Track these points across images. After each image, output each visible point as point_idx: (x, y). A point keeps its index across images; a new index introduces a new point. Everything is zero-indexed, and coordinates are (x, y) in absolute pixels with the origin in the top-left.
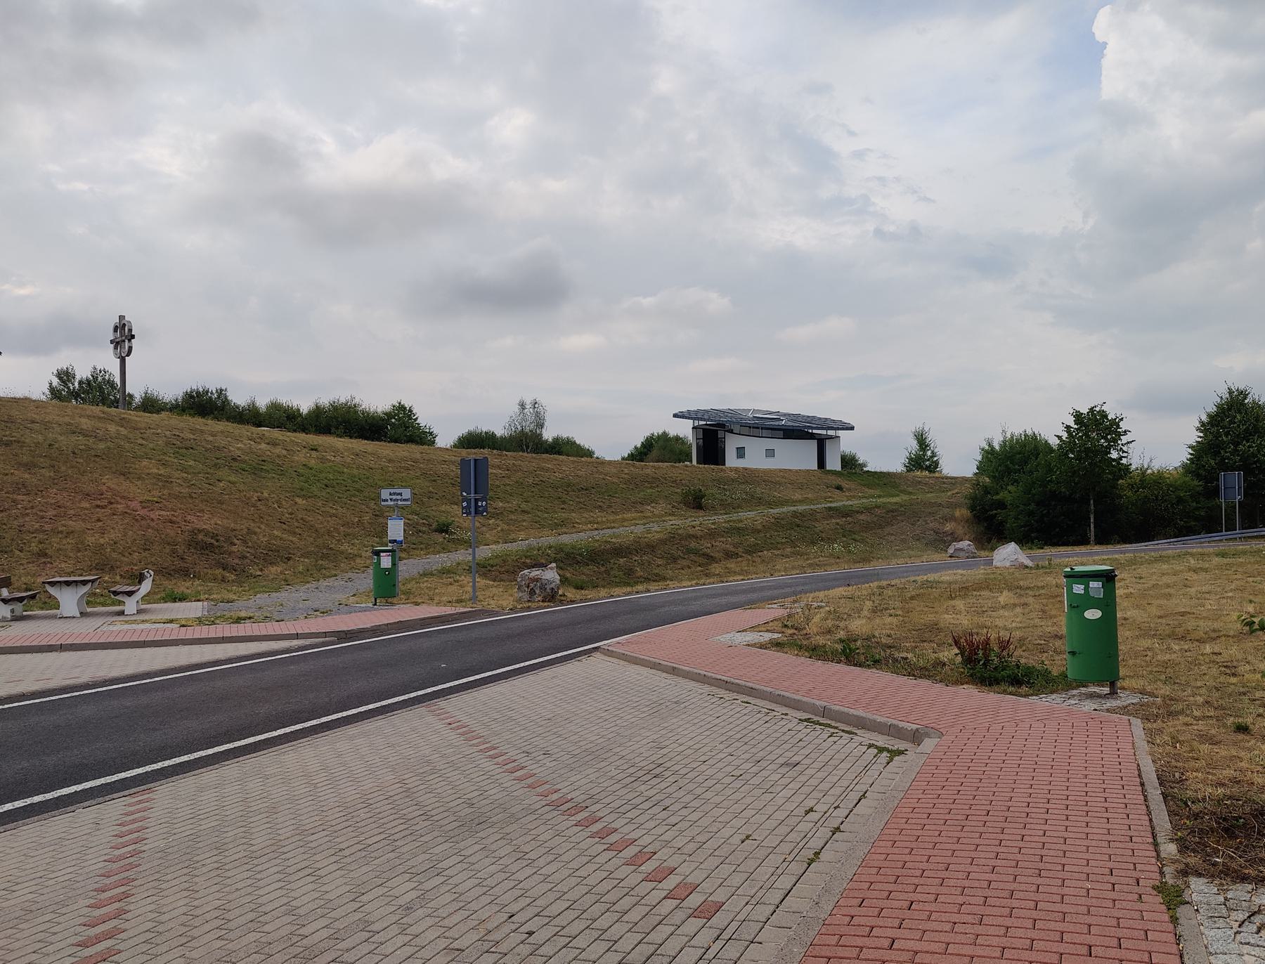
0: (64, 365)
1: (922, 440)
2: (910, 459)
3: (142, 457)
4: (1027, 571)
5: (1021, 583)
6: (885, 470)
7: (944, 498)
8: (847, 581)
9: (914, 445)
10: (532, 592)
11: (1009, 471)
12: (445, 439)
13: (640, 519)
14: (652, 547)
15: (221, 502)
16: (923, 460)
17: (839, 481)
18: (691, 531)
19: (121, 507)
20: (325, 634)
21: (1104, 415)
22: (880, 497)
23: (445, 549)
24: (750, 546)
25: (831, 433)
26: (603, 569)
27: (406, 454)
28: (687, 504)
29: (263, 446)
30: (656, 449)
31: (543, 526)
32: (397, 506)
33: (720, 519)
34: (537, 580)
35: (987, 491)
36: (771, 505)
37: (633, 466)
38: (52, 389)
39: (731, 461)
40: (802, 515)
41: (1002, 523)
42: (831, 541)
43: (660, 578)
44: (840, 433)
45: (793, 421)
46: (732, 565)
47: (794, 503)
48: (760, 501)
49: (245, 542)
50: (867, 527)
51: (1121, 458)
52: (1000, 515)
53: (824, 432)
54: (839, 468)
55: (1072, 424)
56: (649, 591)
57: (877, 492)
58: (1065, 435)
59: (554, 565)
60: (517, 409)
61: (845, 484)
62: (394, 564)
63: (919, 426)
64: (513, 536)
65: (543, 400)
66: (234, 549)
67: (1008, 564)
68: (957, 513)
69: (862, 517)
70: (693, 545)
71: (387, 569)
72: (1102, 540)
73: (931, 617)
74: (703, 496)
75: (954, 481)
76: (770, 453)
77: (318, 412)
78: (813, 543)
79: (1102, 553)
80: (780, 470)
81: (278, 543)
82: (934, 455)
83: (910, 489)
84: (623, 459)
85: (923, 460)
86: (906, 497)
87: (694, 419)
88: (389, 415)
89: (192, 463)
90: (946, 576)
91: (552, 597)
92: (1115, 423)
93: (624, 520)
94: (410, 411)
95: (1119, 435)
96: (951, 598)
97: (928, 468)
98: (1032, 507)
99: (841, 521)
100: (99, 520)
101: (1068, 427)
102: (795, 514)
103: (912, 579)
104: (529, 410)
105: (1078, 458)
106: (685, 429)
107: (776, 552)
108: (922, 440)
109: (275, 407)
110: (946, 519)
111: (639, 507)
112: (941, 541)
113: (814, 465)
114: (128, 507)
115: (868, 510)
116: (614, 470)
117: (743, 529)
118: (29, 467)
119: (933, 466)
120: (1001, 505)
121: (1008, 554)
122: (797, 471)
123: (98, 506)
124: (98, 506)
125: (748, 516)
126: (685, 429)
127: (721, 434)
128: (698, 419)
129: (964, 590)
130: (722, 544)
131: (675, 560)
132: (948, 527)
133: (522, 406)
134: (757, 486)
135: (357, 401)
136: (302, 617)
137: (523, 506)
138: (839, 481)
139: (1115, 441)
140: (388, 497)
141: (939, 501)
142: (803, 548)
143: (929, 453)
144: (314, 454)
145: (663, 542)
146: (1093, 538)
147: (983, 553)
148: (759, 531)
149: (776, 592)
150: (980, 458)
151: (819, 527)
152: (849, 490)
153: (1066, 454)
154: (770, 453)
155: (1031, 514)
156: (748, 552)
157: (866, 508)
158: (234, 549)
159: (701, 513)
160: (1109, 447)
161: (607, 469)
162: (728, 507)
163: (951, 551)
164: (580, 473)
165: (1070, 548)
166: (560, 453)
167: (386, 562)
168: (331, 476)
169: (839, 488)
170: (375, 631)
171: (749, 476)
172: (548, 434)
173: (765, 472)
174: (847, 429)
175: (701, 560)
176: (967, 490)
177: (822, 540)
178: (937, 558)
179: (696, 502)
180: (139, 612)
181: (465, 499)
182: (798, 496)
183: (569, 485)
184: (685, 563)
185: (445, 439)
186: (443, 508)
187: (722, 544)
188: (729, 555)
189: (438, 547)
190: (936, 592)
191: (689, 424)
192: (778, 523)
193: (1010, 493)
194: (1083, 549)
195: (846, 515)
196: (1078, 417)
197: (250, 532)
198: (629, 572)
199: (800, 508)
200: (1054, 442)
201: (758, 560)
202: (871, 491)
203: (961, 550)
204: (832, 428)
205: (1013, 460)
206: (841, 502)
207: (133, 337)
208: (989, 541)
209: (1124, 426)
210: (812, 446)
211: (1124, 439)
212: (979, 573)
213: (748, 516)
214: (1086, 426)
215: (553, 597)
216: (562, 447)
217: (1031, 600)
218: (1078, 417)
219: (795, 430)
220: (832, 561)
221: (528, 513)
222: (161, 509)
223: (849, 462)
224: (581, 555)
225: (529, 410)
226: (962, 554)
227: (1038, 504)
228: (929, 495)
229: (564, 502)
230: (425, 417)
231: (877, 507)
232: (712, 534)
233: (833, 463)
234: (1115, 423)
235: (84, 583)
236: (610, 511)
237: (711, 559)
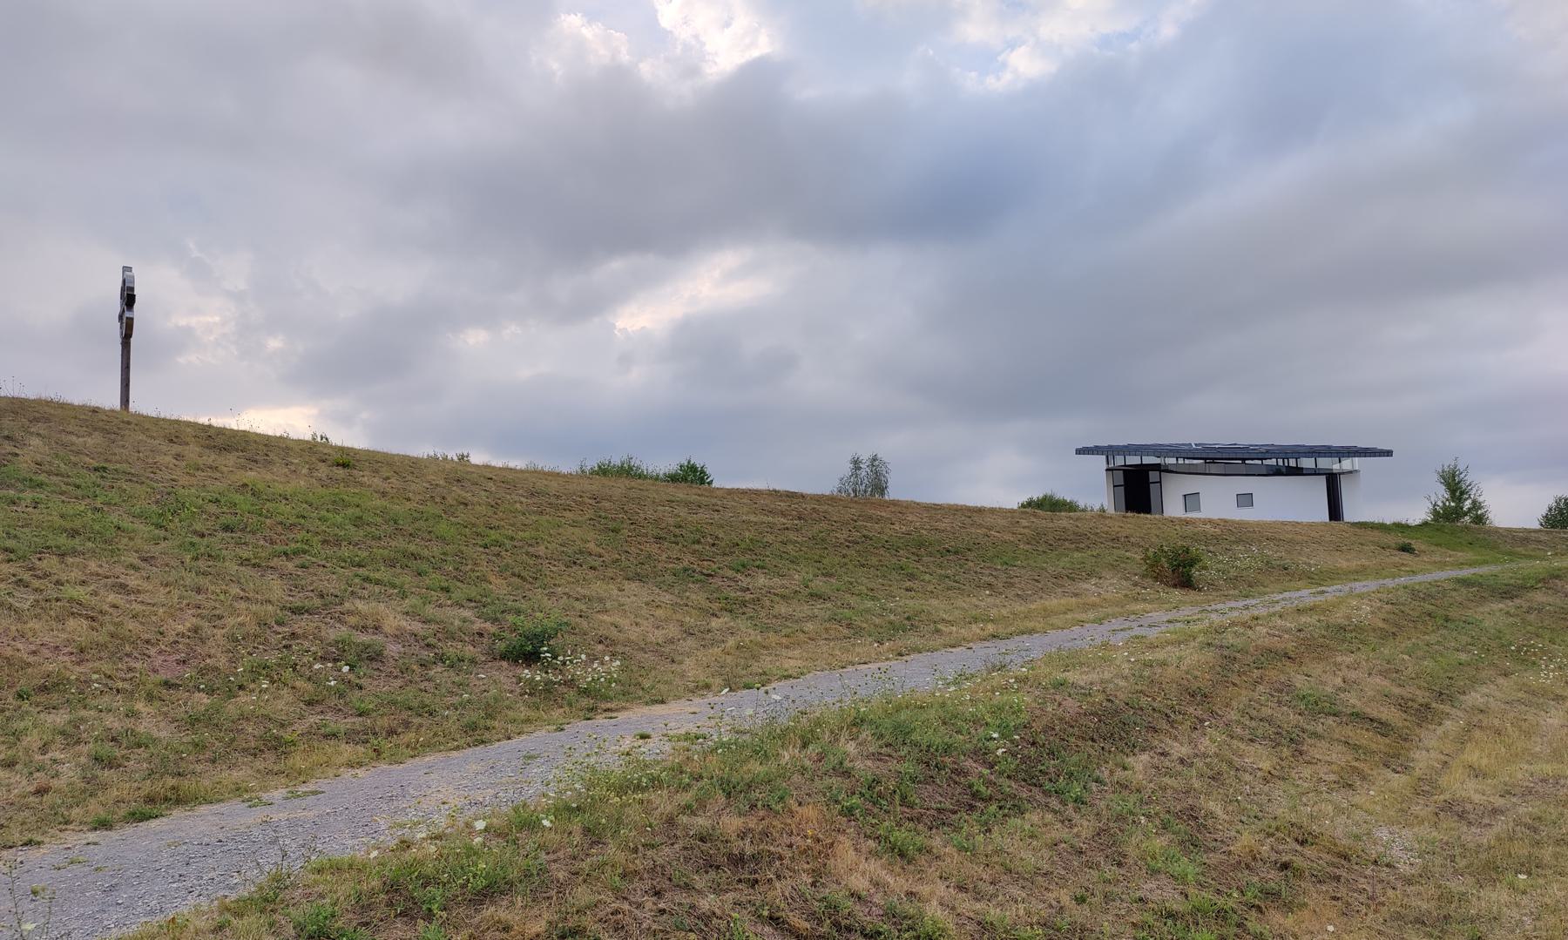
1: (1454, 485)
9: (1441, 494)
25: (1347, 464)
31: (859, 632)
37: (1035, 515)
44: (1357, 463)
45: (910, 623)
57: (1469, 555)
60: (847, 469)
63: (1448, 463)
64: (766, 662)
76: (1245, 500)
82: (1476, 505)
84: (1023, 506)
93: (1047, 613)
94: (702, 472)
113: (1324, 515)
116: (1002, 522)
127: (1153, 476)
133: (856, 463)
137: (819, 584)
143: (1467, 504)
154: (1245, 500)
161: (989, 520)
164: (941, 526)
169: (1405, 549)
183: (920, 545)
186: (598, 588)
219: (1283, 463)
221: (826, 599)
229: (911, 577)
236: (1011, 593)
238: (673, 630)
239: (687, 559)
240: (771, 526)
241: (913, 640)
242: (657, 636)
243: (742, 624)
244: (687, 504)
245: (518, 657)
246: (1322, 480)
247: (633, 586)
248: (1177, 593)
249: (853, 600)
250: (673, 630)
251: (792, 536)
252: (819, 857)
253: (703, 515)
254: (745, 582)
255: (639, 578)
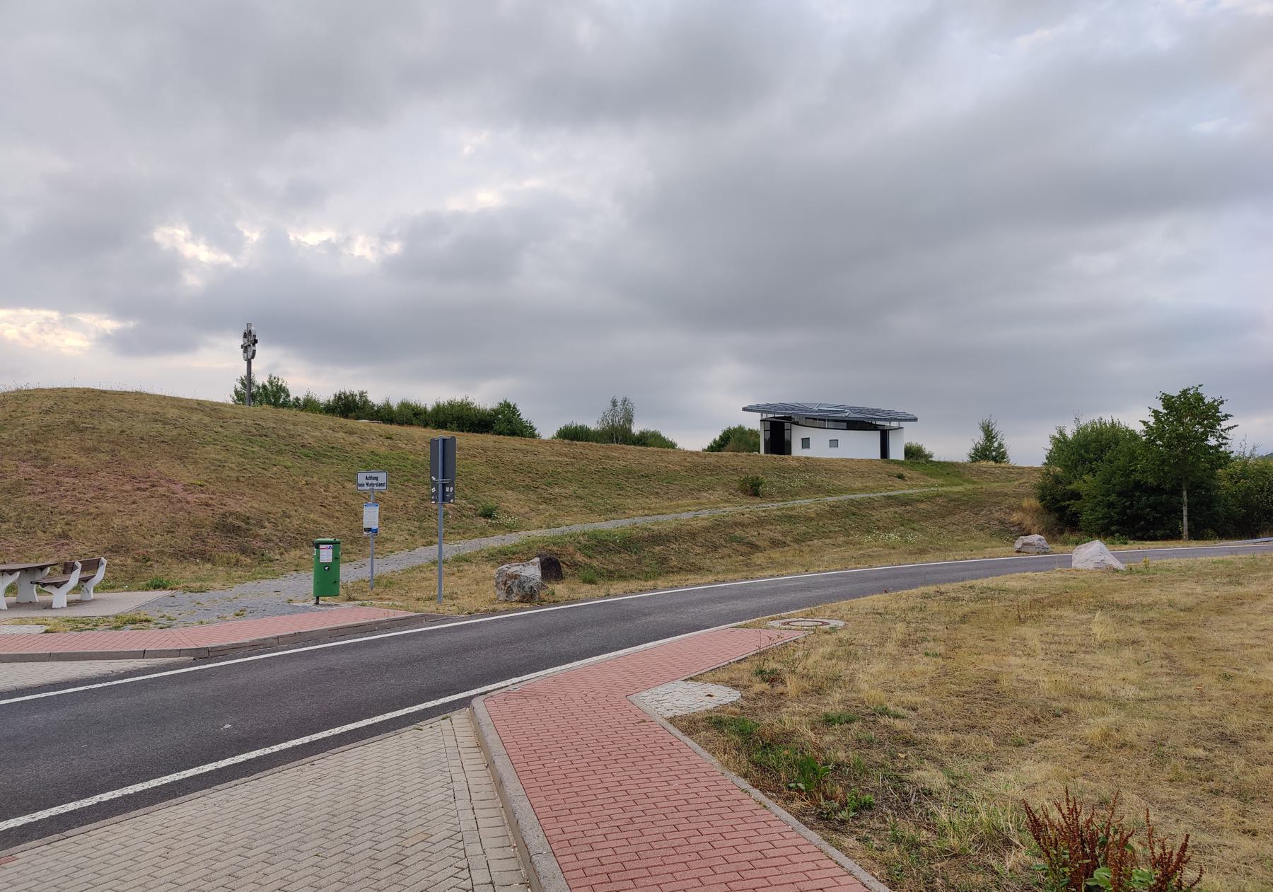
0: (806, 450)
1: (989, 435)
2: (976, 450)
3: (208, 443)
4: (1117, 577)
5: (1117, 597)
6: (948, 459)
7: (1010, 488)
8: (884, 585)
10: (509, 591)
11: (1083, 460)
12: (547, 430)
13: (695, 505)
14: (693, 535)
15: (266, 486)
16: (990, 452)
17: (901, 470)
18: (739, 519)
19: (161, 490)
20: (179, 653)
21: (1200, 399)
22: (942, 486)
23: (483, 534)
24: (800, 535)
25: (894, 424)
26: (635, 557)
27: (479, 443)
28: (745, 492)
29: (341, 434)
30: (732, 440)
32: (373, 491)
33: (773, 507)
34: (515, 577)
35: (1058, 481)
36: (829, 493)
38: (236, 393)
39: (797, 450)
40: (858, 504)
41: (1075, 514)
42: (887, 530)
43: (696, 569)
44: (902, 424)
46: (776, 554)
47: (853, 491)
48: (819, 489)
49: (276, 525)
50: (927, 516)
51: (1220, 446)
52: (1074, 506)
53: (887, 424)
54: (901, 457)
55: (1161, 409)
56: (655, 589)
57: (940, 481)
58: (1152, 421)
59: (537, 559)
60: (609, 405)
61: (906, 473)
62: (336, 558)
64: (560, 521)
65: (632, 399)
66: (262, 532)
67: (1091, 566)
68: (1025, 503)
69: (923, 506)
70: (738, 532)
71: (326, 564)
72: (1196, 535)
73: (987, 663)
74: (760, 484)
75: (1022, 471)
76: (834, 443)
77: (439, 409)
78: (868, 532)
79: (1205, 553)
80: (842, 460)
81: (311, 526)
82: (1000, 445)
83: (974, 479)
85: (990, 452)
86: (969, 487)
87: (762, 412)
88: (497, 412)
89: (256, 449)
90: (1014, 581)
91: (529, 597)
92: (1214, 407)
93: (678, 506)
95: (1219, 420)
96: (1020, 621)
97: (994, 459)
98: (1113, 498)
99: (900, 510)
100: (134, 503)
101: (1156, 413)
102: (852, 503)
103: (969, 583)
104: (619, 407)
105: (1169, 446)
106: (753, 422)
107: (827, 541)
108: (989, 435)
109: (405, 405)
110: (1012, 509)
111: (696, 494)
112: (1011, 531)
113: (879, 457)
114: (169, 490)
115: (929, 499)
116: (678, 459)
117: (794, 517)
118: (88, 451)
119: (1000, 457)
120: (1076, 495)
121: (1092, 554)
122: (859, 461)
123: (139, 489)
124: (139, 489)
125: (805, 504)
126: (753, 422)
127: (787, 426)
128: (767, 412)
129: (1037, 607)
130: (775, 532)
131: (715, 548)
132: (1016, 517)
133: (614, 403)
134: (820, 476)
135: (469, 400)
136: (230, 616)
137: (580, 492)
138: (901, 470)
139: (1212, 427)
140: (365, 482)
141: (1005, 490)
142: (856, 538)
143: (996, 445)
144: (387, 442)
145: (706, 530)
146: (1186, 533)
147: (1057, 548)
148: (811, 519)
149: (800, 595)
150: (1050, 447)
151: (876, 515)
152: (911, 479)
153: (1154, 441)
155: (1111, 505)
156: (797, 541)
157: (926, 497)
158: (262, 532)
159: (758, 500)
160: (1205, 434)
162: (785, 494)
163: (1018, 545)
165: (1160, 544)
166: (645, 444)
167: (326, 555)
168: (392, 462)
169: (901, 477)
170: (256, 647)
171: (811, 465)
172: (636, 429)
173: (827, 461)
174: (910, 420)
175: (743, 549)
176: (1037, 479)
177: (879, 529)
178: (1001, 552)
179: (753, 489)
180: (70, 603)
181: (434, 484)
182: (858, 485)
183: (630, 472)
184: (726, 551)
185: (547, 430)
186: (498, 493)
187: (775, 532)
188: (775, 544)
189: (477, 532)
190: (998, 607)
191: (758, 416)
192: (833, 511)
193: (1085, 483)
194: (1172, 546)
195: (906, 504)
196: (1168, 401)
197: (286, 515)
198: (663, 560)
199: (859, 496)
200: (1139, 428)
201: (806, 549)
202: (934, 481)
203: (1030, 544)
204: (895, 420)
205: (1088, 450)
206: (901, 490)
207: (256, 341)
208: (1061, 532)
209: (1223, 410)
210: (875, 437)
211: (1225, 424)
212: (1052, 579)
213: (805, 504)
214: (1177, 410)
215: (532, 596)
216: (644, 440)
217: (1139, 632)
218: (1168, 401)
220: (887, 551)
222: (202, 492)
223: (913, 454)
224: (614, 542)
225: (619, 407)
226: (1030, 549)
227: (1119, 494)
228: (995, 485)
229: (621, 489)
230: (526, 413)
231: (939, 496)
232: (761, 522)
233: (896, 453)
234: (1214, 407)
235: (11, 572)
237: (754, 547)
238: (527, 509)
239: (527, 480)
240: (560, 462)
241: (613, 515)
242: (522, 511)
243: (550, 507)
244: (522, 451)
245: (1057, 510)
246: (877, 435)
247: (509, 492)
248: (749, 500)
249: (593, 499)
250: (527, 509)
251: (570, 468)
252: (572, 556)
253: (530, 458)
254: (550, 490)
255: (512, 489)
